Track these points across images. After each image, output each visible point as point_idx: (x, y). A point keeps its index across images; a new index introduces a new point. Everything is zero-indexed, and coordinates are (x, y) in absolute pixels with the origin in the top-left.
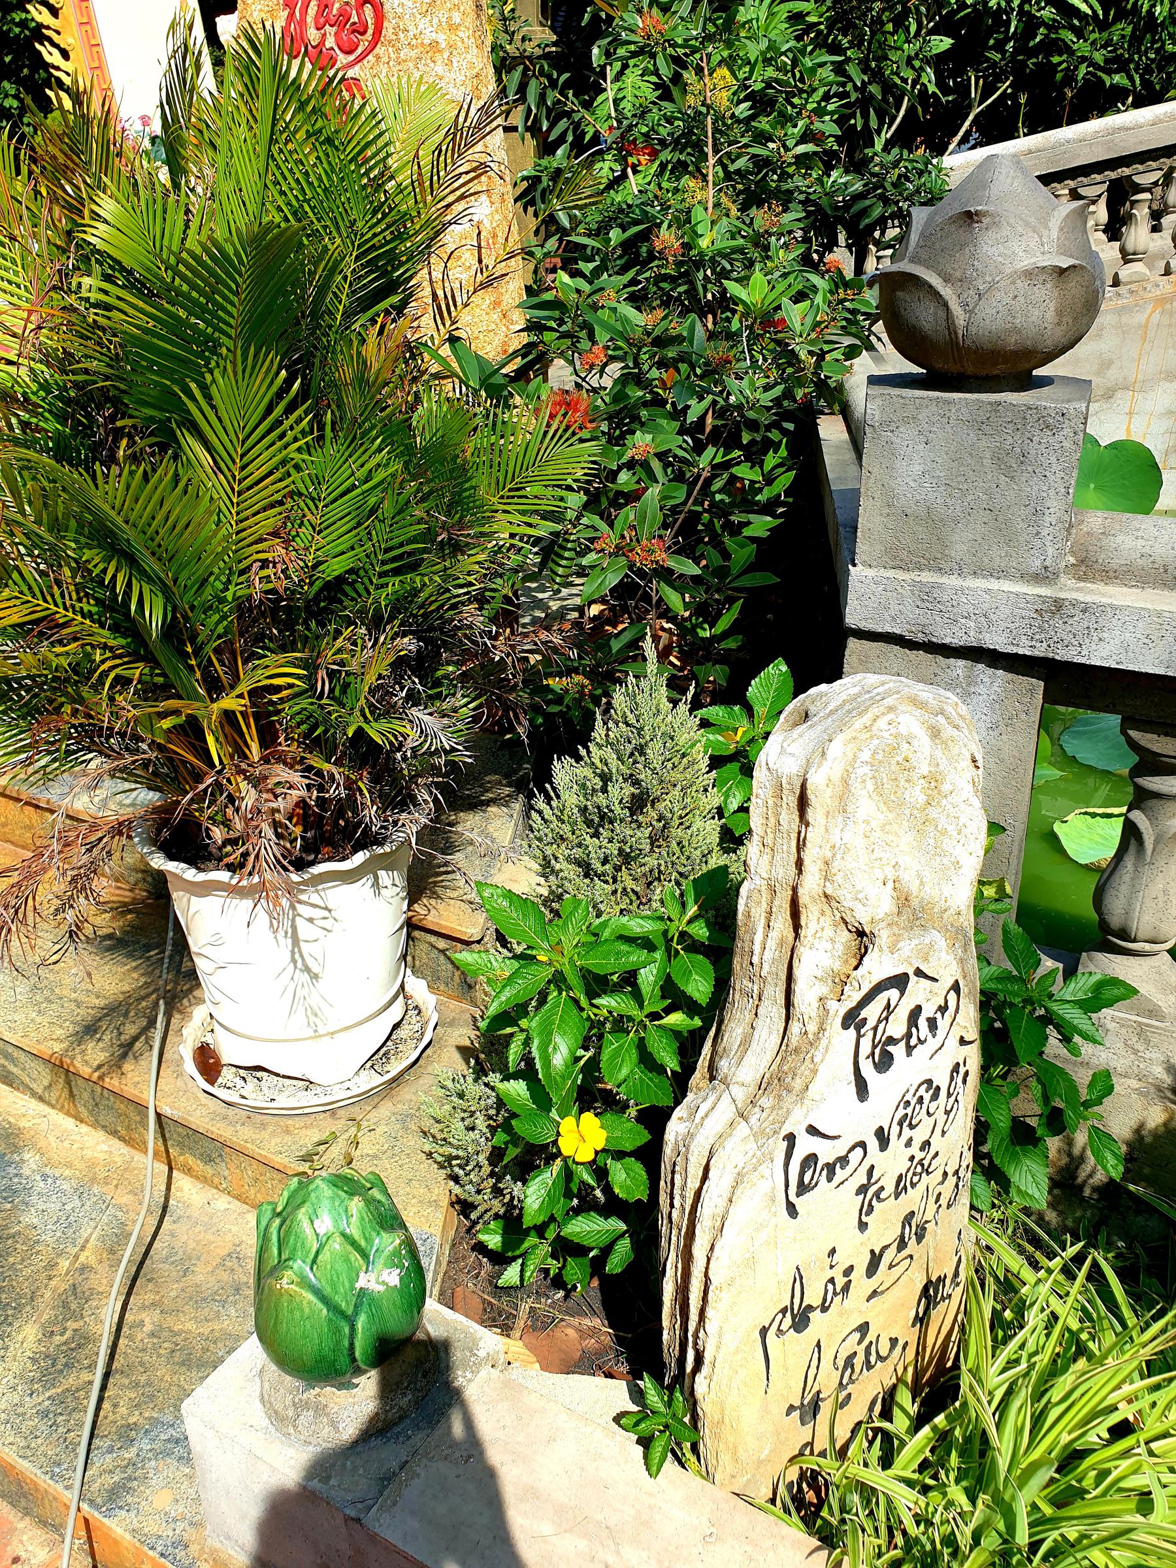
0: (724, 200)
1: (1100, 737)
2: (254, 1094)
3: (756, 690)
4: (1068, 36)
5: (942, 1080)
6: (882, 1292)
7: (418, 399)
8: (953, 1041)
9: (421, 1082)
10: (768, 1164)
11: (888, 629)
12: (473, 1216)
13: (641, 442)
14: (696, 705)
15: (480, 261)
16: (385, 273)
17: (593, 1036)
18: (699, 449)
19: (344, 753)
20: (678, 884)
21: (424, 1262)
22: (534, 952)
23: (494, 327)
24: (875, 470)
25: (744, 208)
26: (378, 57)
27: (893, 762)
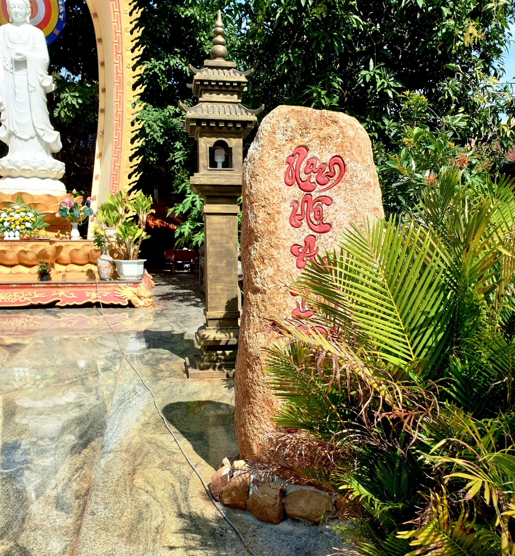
26: (339, 187)
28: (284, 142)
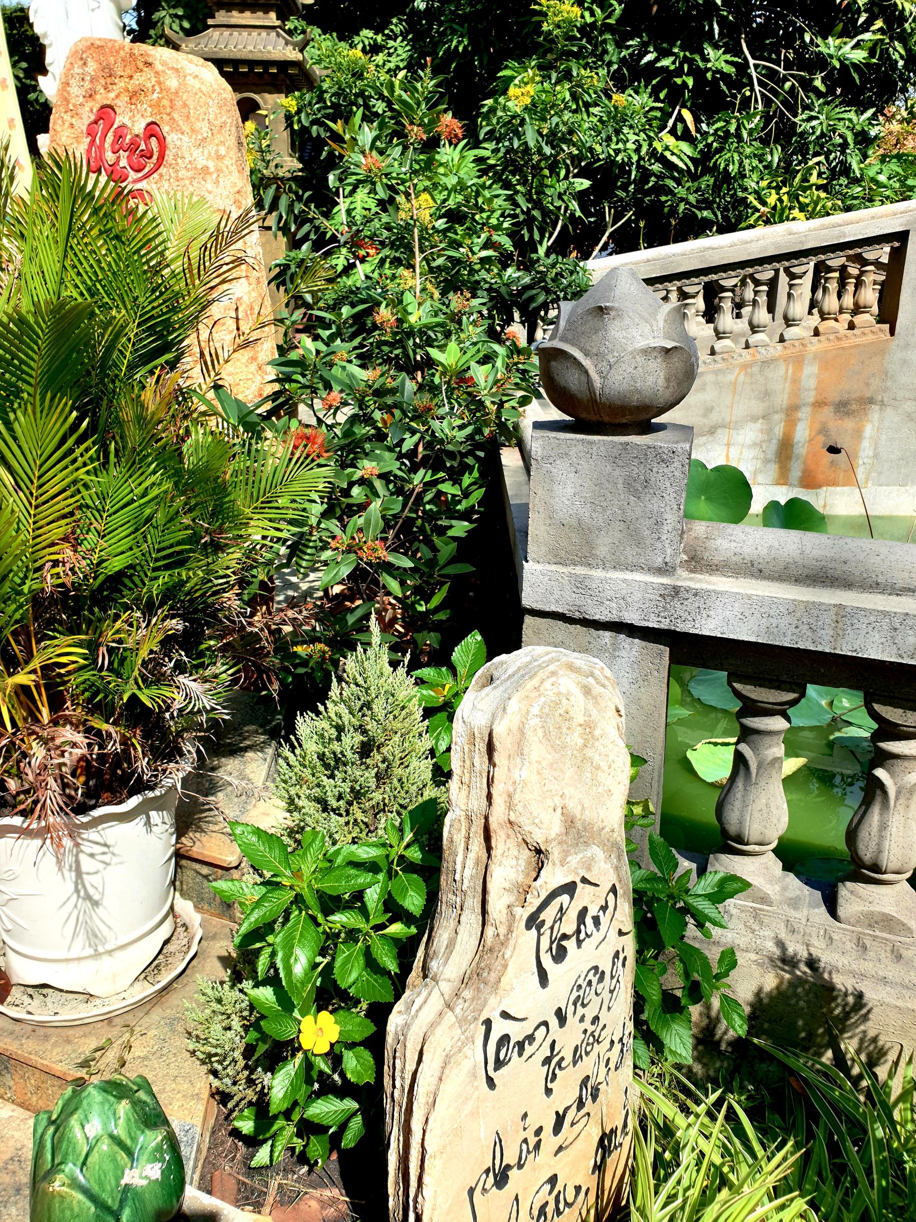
0: (429, 286)
1: (713, 688)
2: (40, 1011)
3: (458, 655)
4: (671, 183)
5: (606, 966)
6: (567, 1147)
7: (188, 433)
8: (613, 933)
9: (187, 989)
10: (470, 1045)
11: (553, 608)
12: (230, 1105)
13: (367, 467)
14: (414, 666)
15: (238, 329)
16: (161, 336)
17: (328, 944)
18: (414, 469)
19: (121, 715)
20: (399, 814)
21: (185, 1151)
22: (278, 879)
23: (250, 379)
24: (540, 492)
25: (444, 294)
26: (161, 176)
27: (557, 714)
28: (81, 99)
